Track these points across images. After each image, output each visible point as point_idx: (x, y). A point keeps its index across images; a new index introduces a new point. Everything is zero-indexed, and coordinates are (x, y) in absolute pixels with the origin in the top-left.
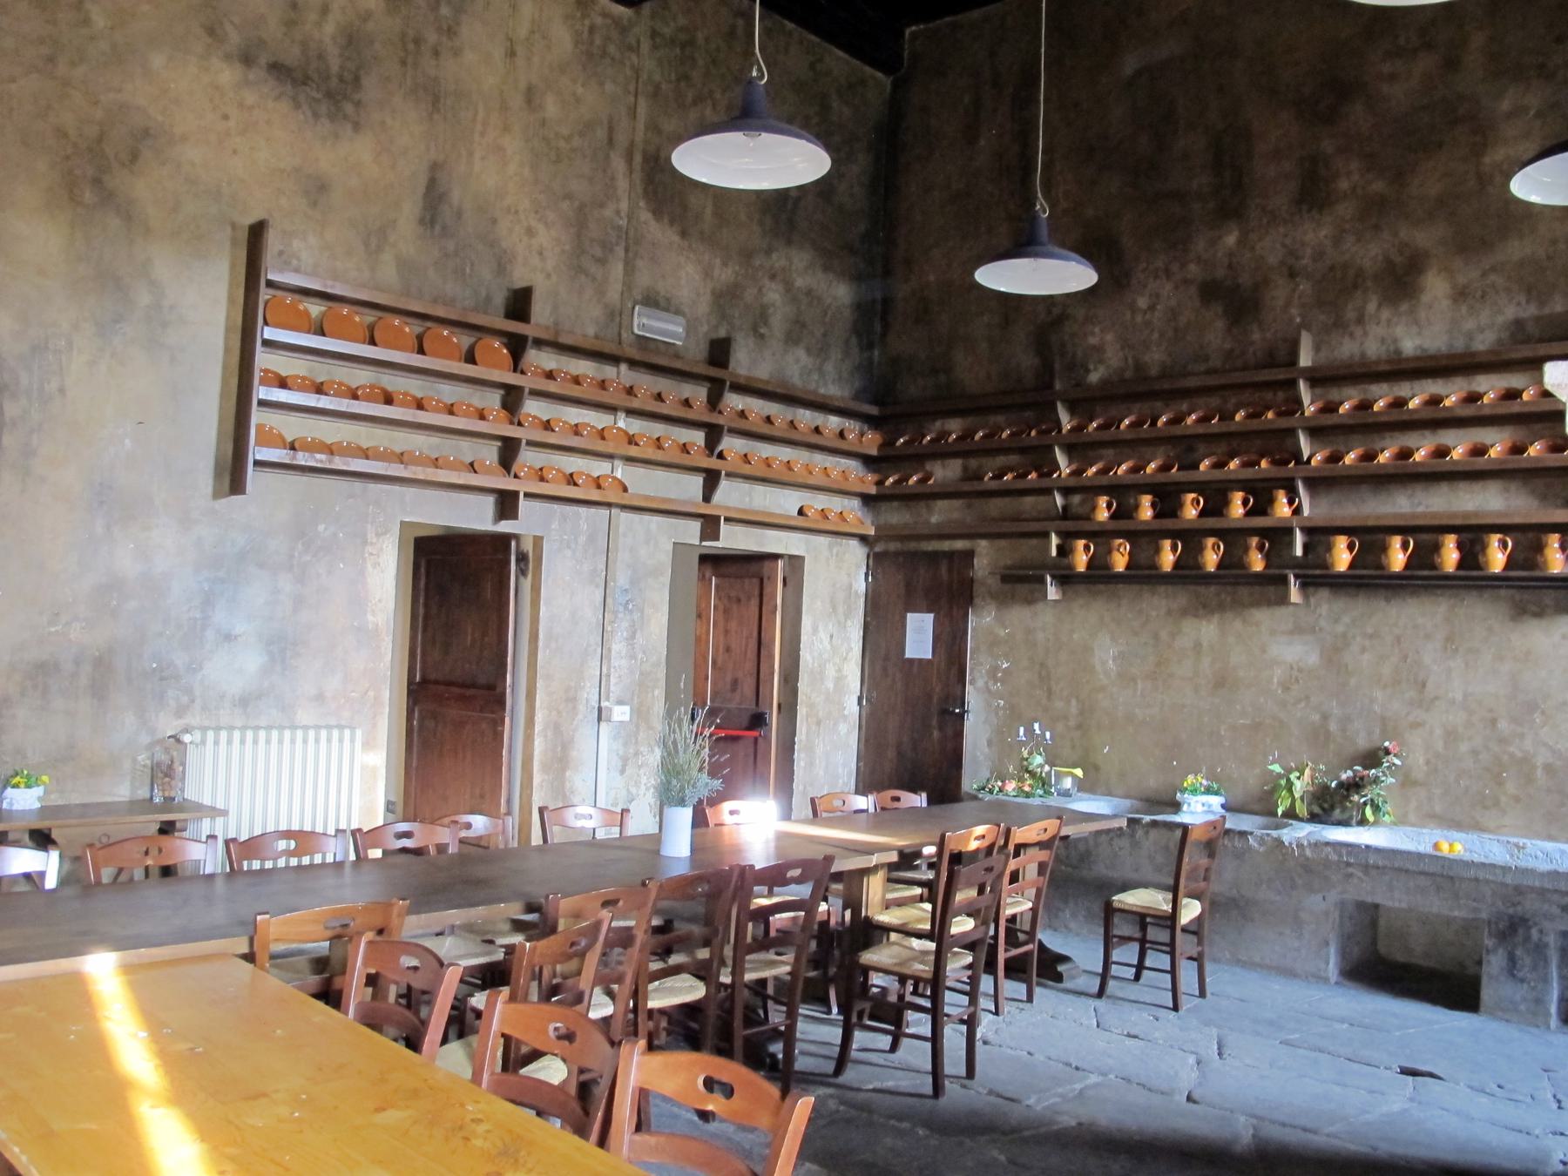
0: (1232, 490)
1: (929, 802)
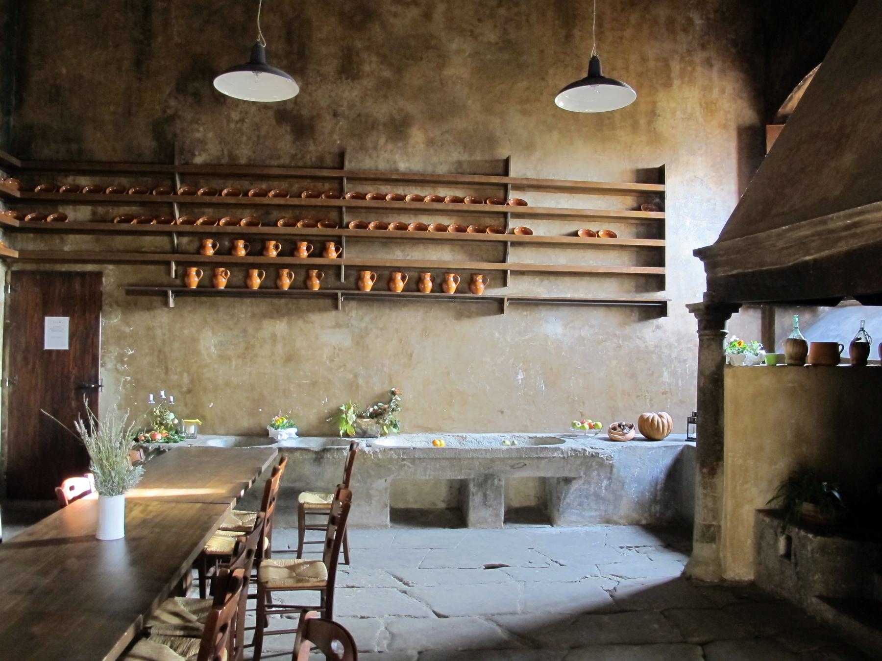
0: (270, 240)
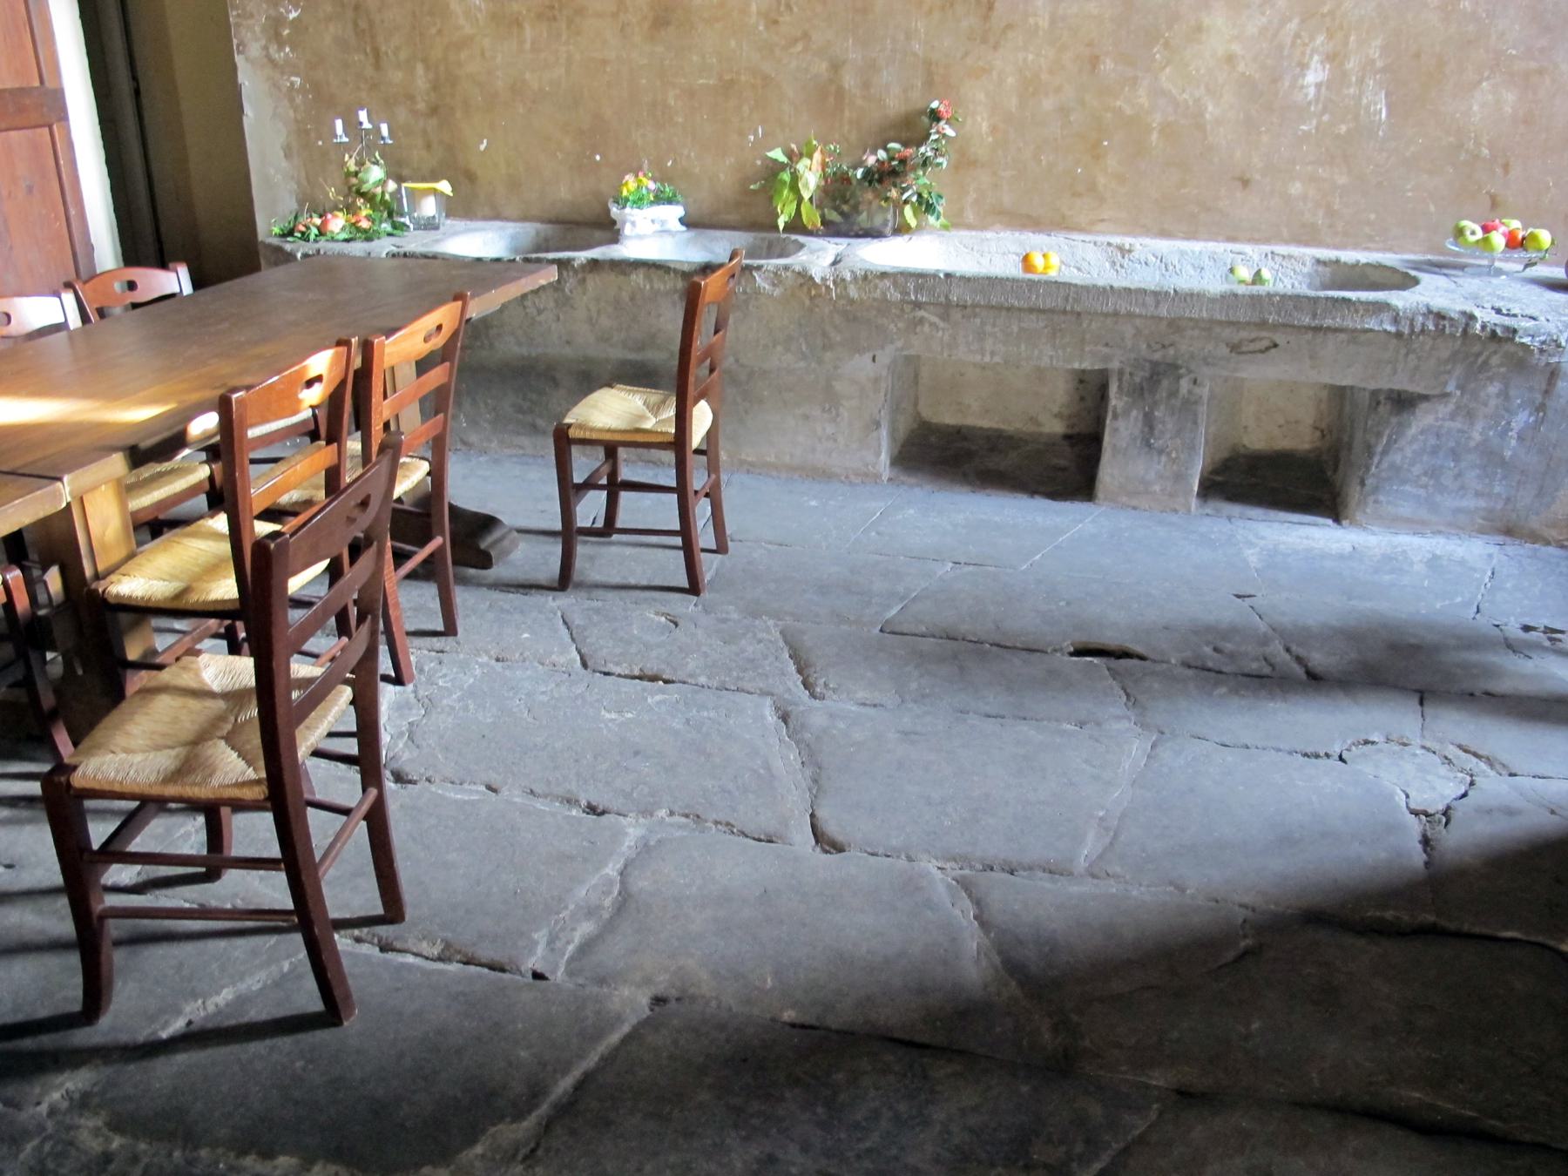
1: (197, 284)
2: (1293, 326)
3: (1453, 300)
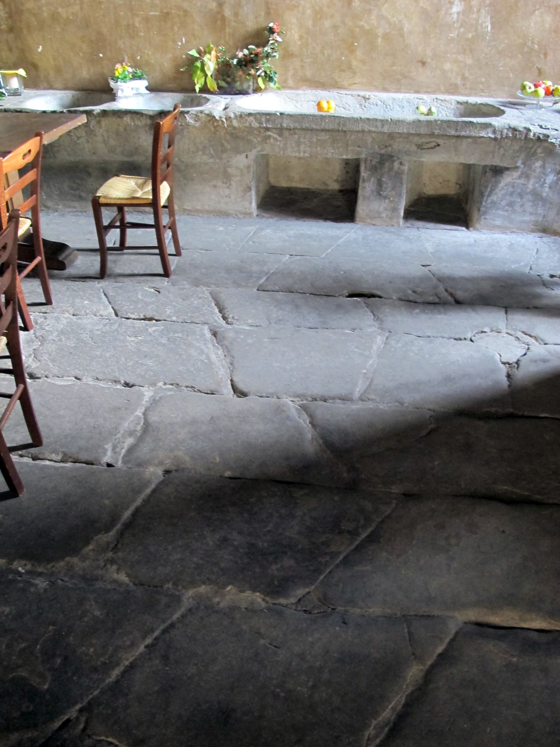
2: (447, 136)
3: (520, 121)
